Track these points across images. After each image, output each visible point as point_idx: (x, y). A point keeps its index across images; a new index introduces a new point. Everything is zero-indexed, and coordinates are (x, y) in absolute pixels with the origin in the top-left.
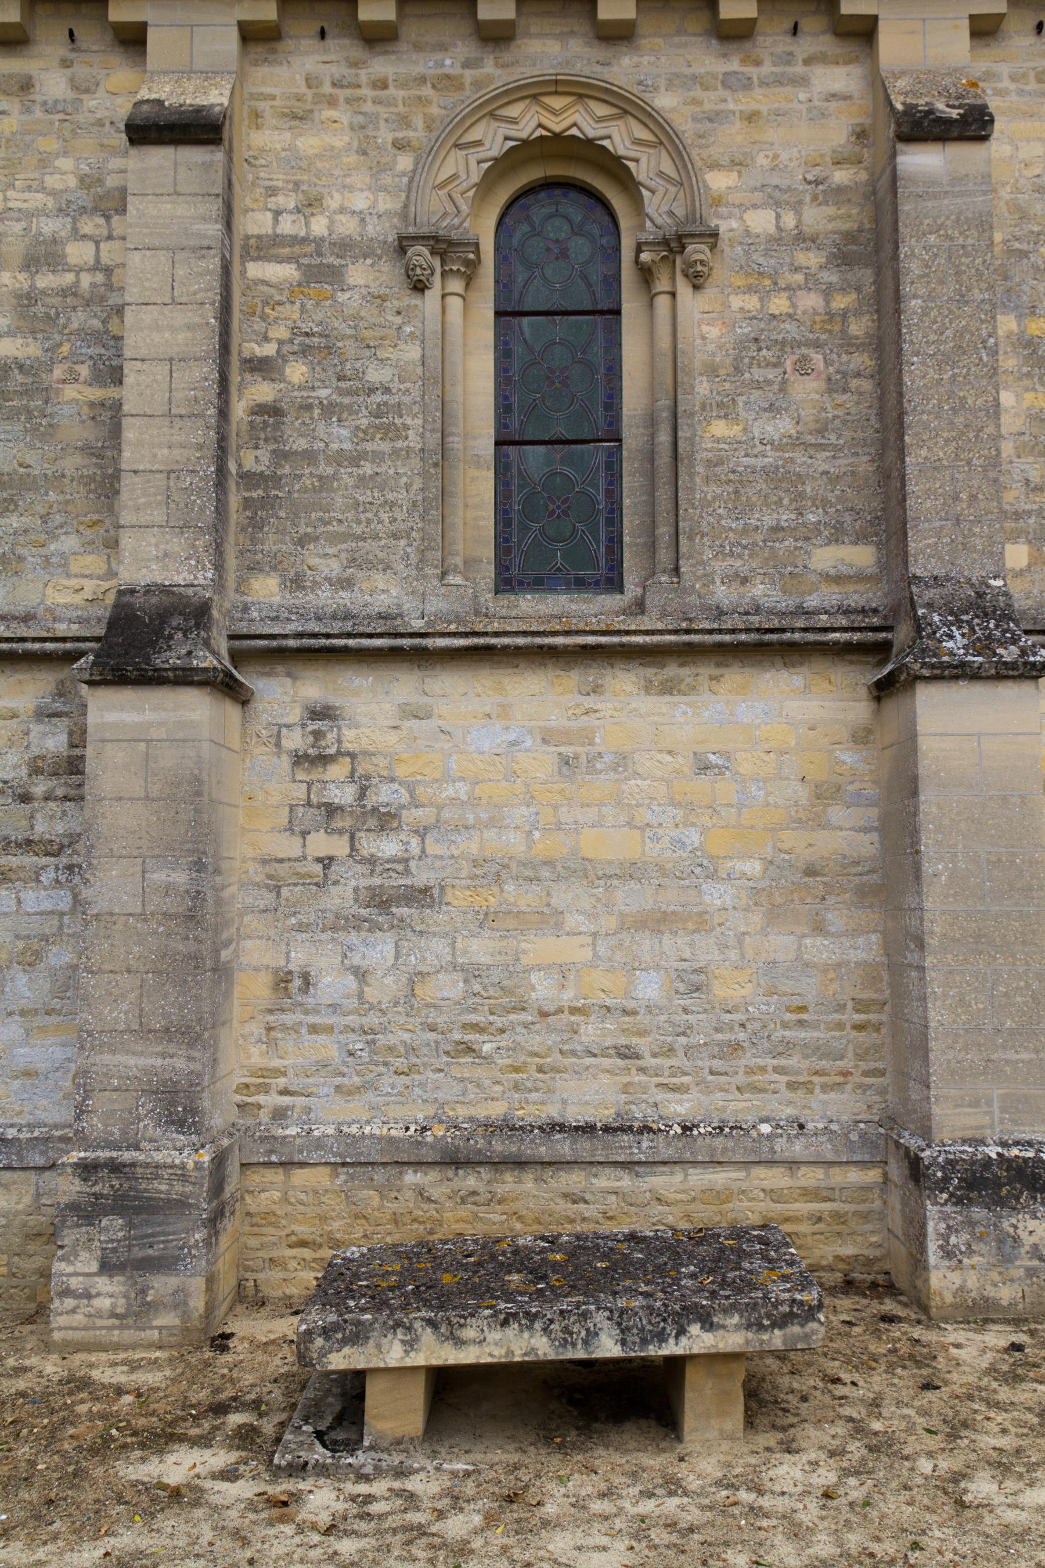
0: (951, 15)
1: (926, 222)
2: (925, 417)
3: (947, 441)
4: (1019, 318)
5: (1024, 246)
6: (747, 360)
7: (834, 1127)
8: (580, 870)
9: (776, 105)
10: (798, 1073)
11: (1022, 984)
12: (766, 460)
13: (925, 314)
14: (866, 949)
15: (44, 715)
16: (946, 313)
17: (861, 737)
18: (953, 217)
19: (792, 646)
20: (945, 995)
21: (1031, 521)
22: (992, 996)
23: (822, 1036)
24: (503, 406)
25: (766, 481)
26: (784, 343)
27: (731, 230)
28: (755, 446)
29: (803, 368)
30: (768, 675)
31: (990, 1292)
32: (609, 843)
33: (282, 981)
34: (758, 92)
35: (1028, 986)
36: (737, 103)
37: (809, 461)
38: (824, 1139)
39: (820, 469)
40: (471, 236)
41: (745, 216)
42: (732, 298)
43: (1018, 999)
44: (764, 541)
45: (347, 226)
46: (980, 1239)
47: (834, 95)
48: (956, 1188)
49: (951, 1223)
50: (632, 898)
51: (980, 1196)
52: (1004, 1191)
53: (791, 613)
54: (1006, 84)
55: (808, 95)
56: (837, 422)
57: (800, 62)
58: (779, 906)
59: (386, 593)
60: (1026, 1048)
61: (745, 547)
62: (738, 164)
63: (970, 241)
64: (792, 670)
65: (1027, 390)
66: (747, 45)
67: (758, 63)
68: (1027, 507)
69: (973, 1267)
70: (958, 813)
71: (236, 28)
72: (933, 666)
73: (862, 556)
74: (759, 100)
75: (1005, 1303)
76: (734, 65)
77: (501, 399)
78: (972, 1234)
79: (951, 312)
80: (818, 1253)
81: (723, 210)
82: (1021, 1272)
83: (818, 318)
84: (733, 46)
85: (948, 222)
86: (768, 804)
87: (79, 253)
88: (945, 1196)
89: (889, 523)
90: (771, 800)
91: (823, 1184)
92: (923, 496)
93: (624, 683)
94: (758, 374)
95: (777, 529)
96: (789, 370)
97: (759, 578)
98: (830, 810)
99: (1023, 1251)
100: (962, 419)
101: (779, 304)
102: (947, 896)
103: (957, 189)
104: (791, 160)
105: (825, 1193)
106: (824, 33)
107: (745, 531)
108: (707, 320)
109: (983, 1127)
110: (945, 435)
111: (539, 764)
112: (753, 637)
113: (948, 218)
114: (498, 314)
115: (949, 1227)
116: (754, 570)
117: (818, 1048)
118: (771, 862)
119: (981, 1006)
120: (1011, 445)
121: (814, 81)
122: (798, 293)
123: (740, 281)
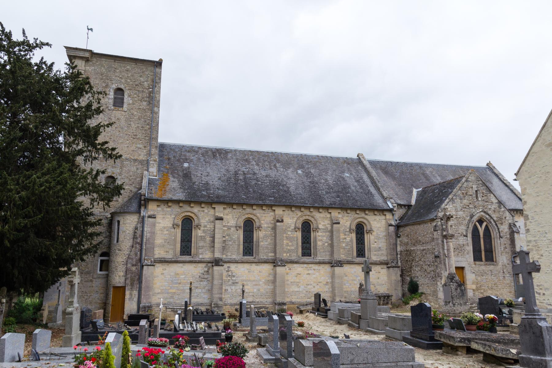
8: (250, 281)
14: (272, 287)
15: (205, 267)
17: (273, 269)
32: (252, 278)
33: (225, 290)
36: (264, 215)
45: (231, 225)
50: (254, 283)
59: (234, 257)
62: (264, 220)
73: (273, 254)
87: (208, 226)
89: (275, 252)
92: (278, 251)
93: (254, 265)
108: (261, 234)
111: (247, 271)
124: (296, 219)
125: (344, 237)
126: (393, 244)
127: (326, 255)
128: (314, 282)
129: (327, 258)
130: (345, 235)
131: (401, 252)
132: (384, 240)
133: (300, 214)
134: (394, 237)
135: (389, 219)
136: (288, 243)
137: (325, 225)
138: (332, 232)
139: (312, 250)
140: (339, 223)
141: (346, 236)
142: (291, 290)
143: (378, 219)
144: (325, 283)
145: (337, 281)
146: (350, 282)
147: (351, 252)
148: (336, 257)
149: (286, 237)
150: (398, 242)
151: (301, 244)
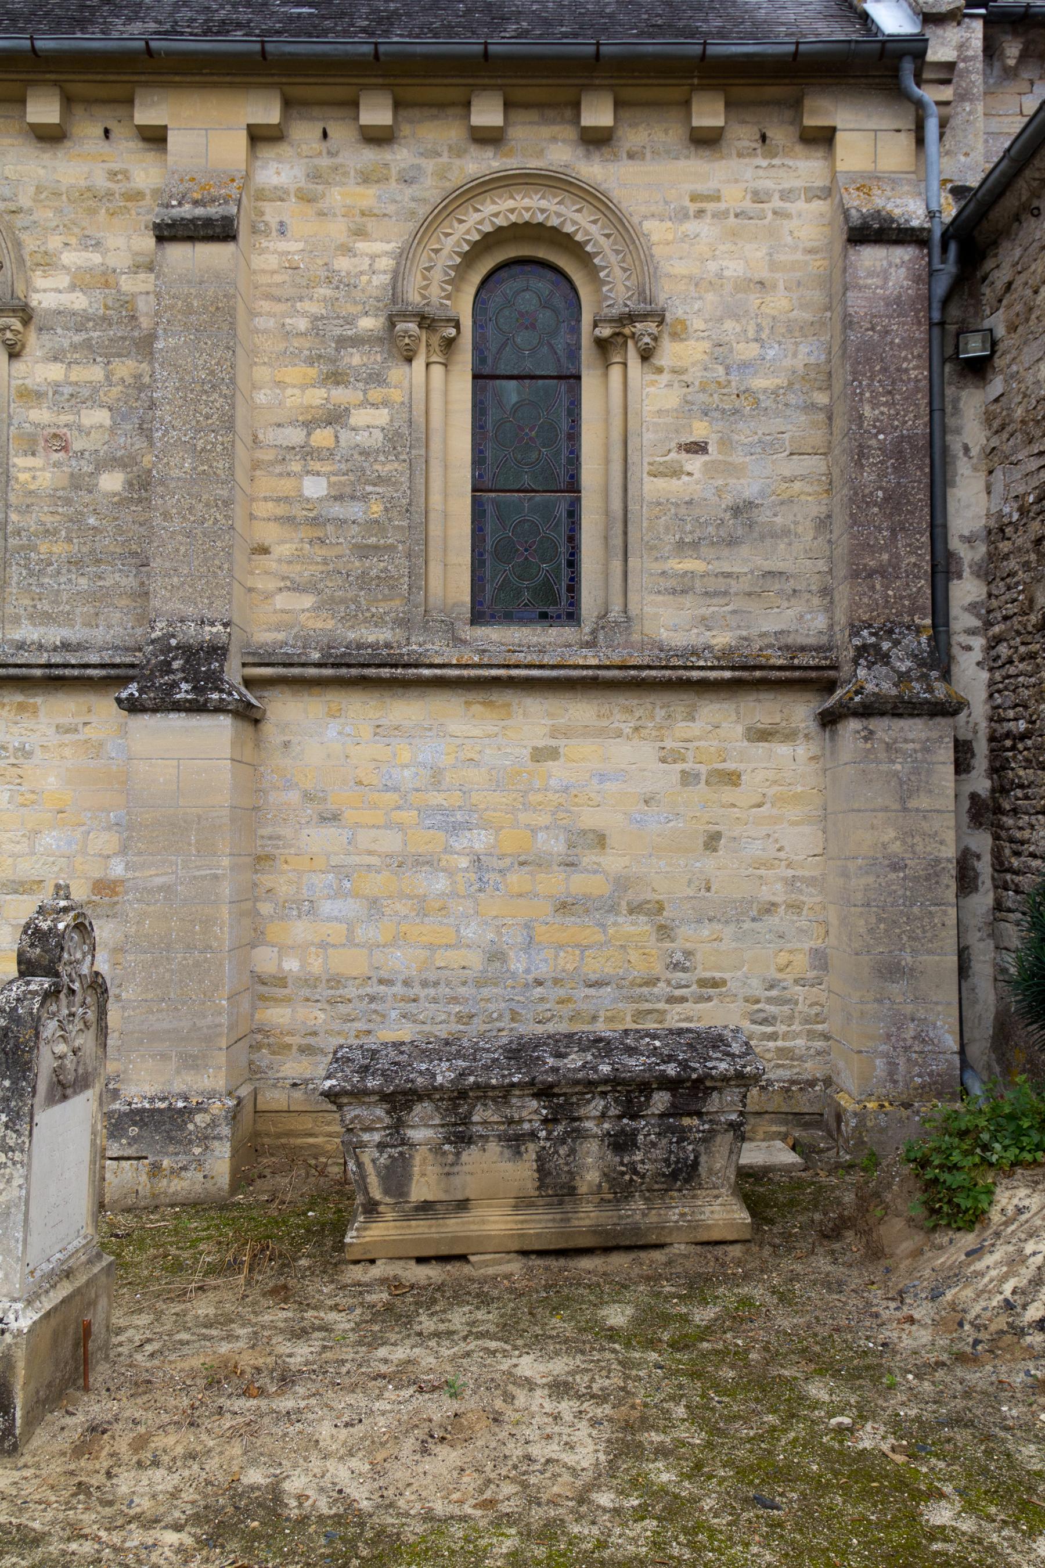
24: (478, 459)
40: (452, 314)
71: (245, 132)
112: (103, 672)
114: (475, 377)
125: (316, 396)
126: (897, 453)
127: (99, 597)
130: (336, 378)
131: (998, 532)
132: (797, 426)
134: (916, 371)
135: (865, 183)
137: (106, 278)
141: (341, 395)
143: (734, 197)
146: (376, 883)
147: (398, 565)
150: (971, 431)
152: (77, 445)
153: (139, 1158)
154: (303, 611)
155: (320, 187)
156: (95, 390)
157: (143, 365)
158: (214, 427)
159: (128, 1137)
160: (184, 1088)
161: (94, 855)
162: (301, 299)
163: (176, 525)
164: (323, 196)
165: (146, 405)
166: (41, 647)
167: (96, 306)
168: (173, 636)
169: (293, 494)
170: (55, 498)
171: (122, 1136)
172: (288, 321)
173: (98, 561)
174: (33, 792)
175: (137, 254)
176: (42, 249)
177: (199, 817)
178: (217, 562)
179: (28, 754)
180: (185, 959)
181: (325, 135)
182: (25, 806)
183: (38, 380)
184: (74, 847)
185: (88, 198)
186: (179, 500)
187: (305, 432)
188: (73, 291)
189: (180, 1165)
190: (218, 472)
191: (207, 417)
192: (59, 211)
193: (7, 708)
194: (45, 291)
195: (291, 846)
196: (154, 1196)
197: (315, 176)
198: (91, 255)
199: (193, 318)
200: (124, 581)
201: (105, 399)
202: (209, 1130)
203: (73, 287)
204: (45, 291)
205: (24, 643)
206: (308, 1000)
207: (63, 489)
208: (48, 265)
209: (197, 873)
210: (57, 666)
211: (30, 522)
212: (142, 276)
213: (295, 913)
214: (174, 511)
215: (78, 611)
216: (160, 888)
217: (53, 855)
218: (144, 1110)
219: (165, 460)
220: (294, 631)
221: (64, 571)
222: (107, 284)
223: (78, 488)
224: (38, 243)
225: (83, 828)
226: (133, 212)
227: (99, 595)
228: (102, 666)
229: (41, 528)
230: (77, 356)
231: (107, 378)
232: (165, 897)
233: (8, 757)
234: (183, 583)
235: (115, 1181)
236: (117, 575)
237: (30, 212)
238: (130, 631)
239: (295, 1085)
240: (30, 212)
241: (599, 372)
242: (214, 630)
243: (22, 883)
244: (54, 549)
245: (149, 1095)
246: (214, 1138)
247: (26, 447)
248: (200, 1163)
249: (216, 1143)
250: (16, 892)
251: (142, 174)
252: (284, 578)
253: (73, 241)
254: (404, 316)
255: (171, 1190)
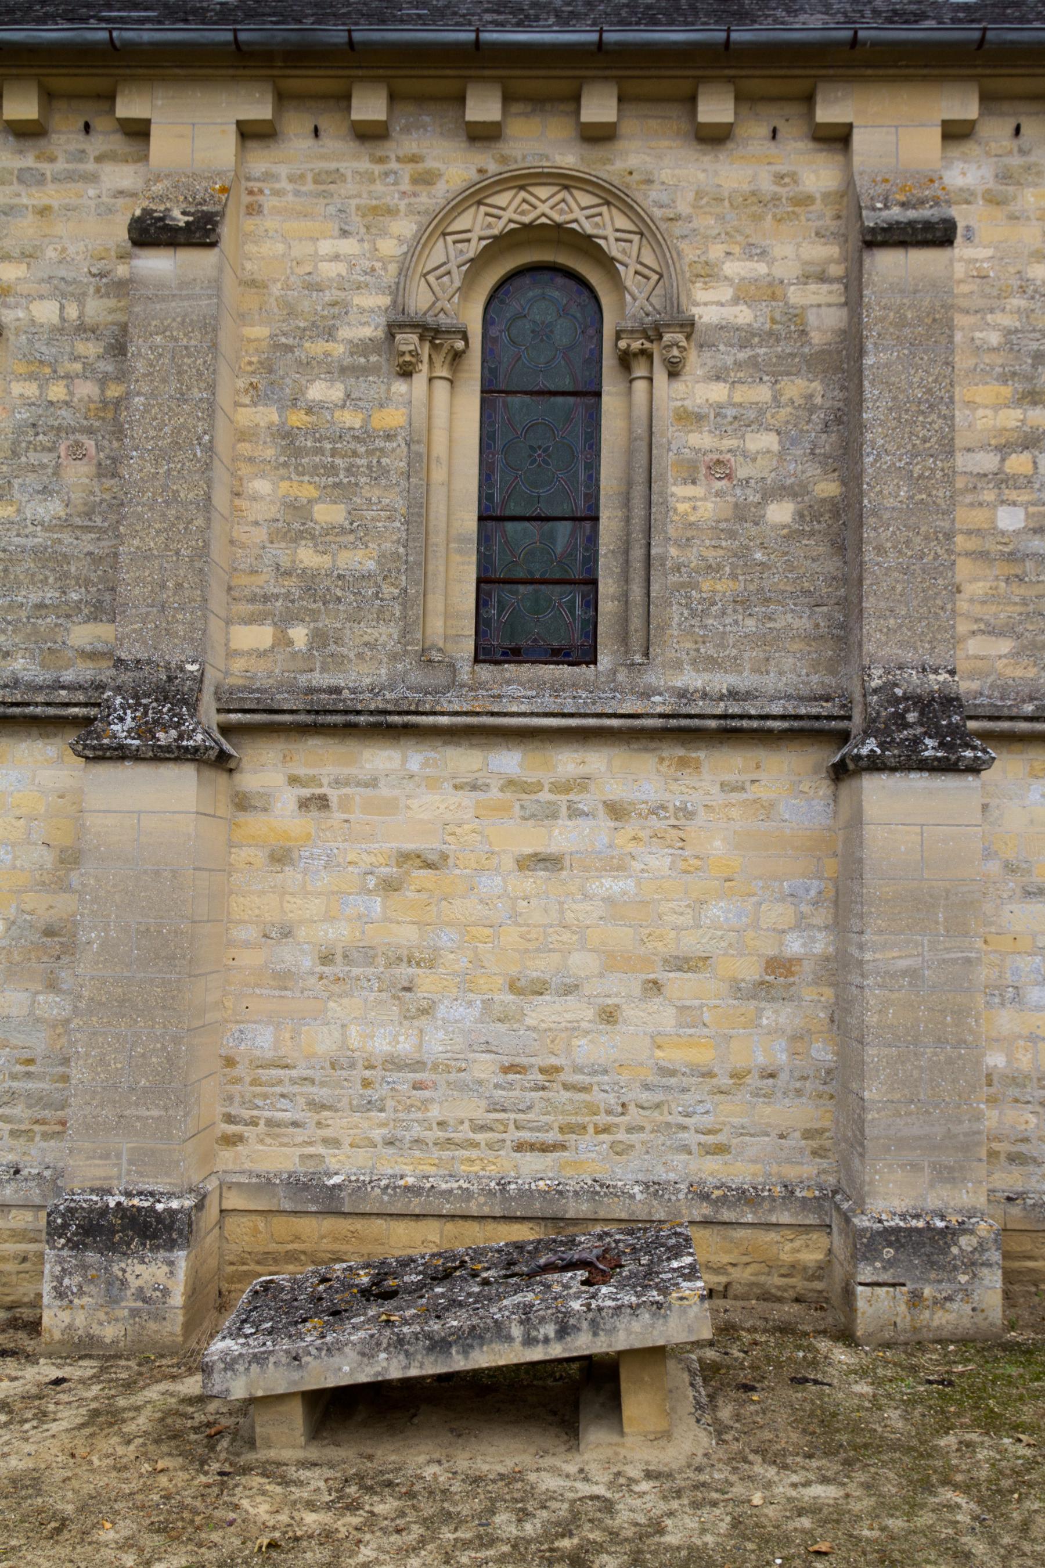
0: (219, 121)
1: (154, 323)
2: (139, 509)
3: (158, 532)
4: (281, 409)
5: (290, 341)
6: (24, 445)
7: (47, 1173)
9: (67, 201)
10: (21, 1122)
11: (159, 1046)
12: (36, 540)
13: (147, 411)
16: (166, 410)
18: (179, 319)
19: (35, 721)
20: (87, 1055)
21: (278, 604)
22: (131, 1057)
23: (47, 1087)
25: (34, 560)
26: (59, 429)
27: (18, 320)
28: (26, 526)
29: (77, 453)
30: (24, 745)
31: (96, 1330)
34: (51, 188)
35: (164, 1048)
36: (31, 198)
37: (75, 542)
38: (33, 1184)
39: (86, 550)
41: (31, 307)
42: (13, 385)
43: (154, 1060)
44: (28, 618)
46: (91, 1281)
47: (121, 192)
48: (74, 1234)
49: (66, 1266)
51: (95, 1242)
52: (117, 1237)
53: (48, 687)
54: (284, 184)
55: (98, 192)
56: (104, 505)
57: (92, 159)
58: (18, 964)
60: (157, 1106)
61: (9, 623)
62: (28, 256)
63: (193, 342)
64: (47, 741)
65: (282, 479)
66: (43, 142)
67: (52, 160)
68: (276, 591)
69: (83, 1307)
70: (114, 886)
72: (94, 748)
74: (52, 195)
75: (108, 1341)
76: (29, 161)
77: (486, 371)
78: (84, 1276)
79: (170, 409)
80: (21, 1290)
81: (10, 300)
82: (126, 1312)
83: (92, 406)
84: (29, 143)
85: (174, 324)
86: (14, 868)
88: (63, 1241)
90: (18, 863)
91: (30, 1227)
94: (33, 458)
95: (40, 606)
96: (62, 454)
97: (21, 653)
98: (72, 874)
99: (129, 1293)
100: (173, 512)
101: (57, 392)
102: (97, 963)
103: (184, 292)
104: (77, 253)
105: (32, 1235)
106: (115, 132)
107: (11, 607)
109: (110, 1178)
110: (157, 526)
113: (174, 320)
115: (63, 1270)
116: (16, 645)
117: (41, 1099)
118: (13, 923)
119: (119, 1066)
120: (265, 531)
121: (104, 178)
122: (76, 381)
123: (22, 369)
124: (406, 227)
125: (1011, 418)
128: (614, 961)
129: (781, 678)
133: (456, 167)
136: (298, 509)
137: (770, 290)
138: (844, 361)
139: (607, 586)
140: (939, 235)
142: (324, 1041)
144: (750, 971)
145: (884, 952)
148: (892, 652)
149: (286, 436)
151: (469, 521)
152: (742, 473)
153: (894, 1285)
154: (1000, 657)
155: (1011, 188)
156: (761, 412)
157: (814, 384)
158: (932, 451)
159: (883, 1260)
160: (939, 1204)
161: (768, 929)
162: (992, 311)
163: (891, 560)
164: (1015, 198)
165: (818, 428)
166: (705, 695)
167: (761, 320)
168: (896, 685)
169: (986, 526)
170: (720, 530)
171: (875, 1259)
172: (978, 335)
173: (767, 601)
174: (697, 857)
175: (807, 263)
176: (703, 258)
177: (947, 891)
178: (939, 602)
179: (690, 815)
180: (936, 1054)
181: (1017, 131)
182: (689, 872)
183: (699, 401)
184: (744, 919)
185: (753, 204)
186: (894, 533)
187: (998, 458)
188: (737, 304)
189: (944, 1294)
190: (939, 501)
191: (925, 440)
192: (721, 218)
193: (667, 763)
194: (705, 304)
195: (991, 924)
196: (915, 1330)
197: (1005, 176)
198: (755, 265)
199: (907, 331)
200: (797, 623)
201: (772, 421)
202: (977, 1256)
203: (736, 300)
204: (705, 304)
205: (686, 691)
206: (1016, 1101)
207: (726, 520)
208: (709, 276)
209: (947, 956)
210: (733, 717)
211: (692, 557)
212: (813, 287)
213: (997, 1000)
214: (889, 545)
215: (746, 655)
216: (905, 973)
217: (721, 928)
218: (897, 1230)
219: (878, 488)
220: (989, 680)
221: (729, 611)
222: (773, 297)
223: (742, 519)
224: (698, 252)
225: (755, 899)
226: (802, 218)
227: (769, 638)
228: (783, 717)
229: (703, 564)
230: (742, 375)
231: (775, 398)
232: (910, 983)
233: (667, 818)
234: (900, 626)
235: (870, 1311)
236: (789, 615)
237: (689, 219)
238: (805, 678)
239: (1009, 1199)
240: (689, 219)
241: (622, 387)
242: (941, 678)
243: (687, 960)
244: (718, 587)
245: (898, 1211)
246: (982, 1264)
247: (685, 475)
248: (967, 1294)
249: (985, 1271)
250: (680, 969)
251: (812, 177)
252: (977, 620)
253: (736, 250)
254: (402, 326)
255: (935, 1323)
